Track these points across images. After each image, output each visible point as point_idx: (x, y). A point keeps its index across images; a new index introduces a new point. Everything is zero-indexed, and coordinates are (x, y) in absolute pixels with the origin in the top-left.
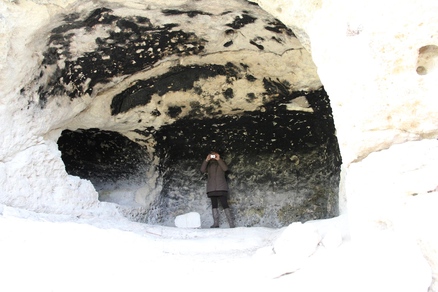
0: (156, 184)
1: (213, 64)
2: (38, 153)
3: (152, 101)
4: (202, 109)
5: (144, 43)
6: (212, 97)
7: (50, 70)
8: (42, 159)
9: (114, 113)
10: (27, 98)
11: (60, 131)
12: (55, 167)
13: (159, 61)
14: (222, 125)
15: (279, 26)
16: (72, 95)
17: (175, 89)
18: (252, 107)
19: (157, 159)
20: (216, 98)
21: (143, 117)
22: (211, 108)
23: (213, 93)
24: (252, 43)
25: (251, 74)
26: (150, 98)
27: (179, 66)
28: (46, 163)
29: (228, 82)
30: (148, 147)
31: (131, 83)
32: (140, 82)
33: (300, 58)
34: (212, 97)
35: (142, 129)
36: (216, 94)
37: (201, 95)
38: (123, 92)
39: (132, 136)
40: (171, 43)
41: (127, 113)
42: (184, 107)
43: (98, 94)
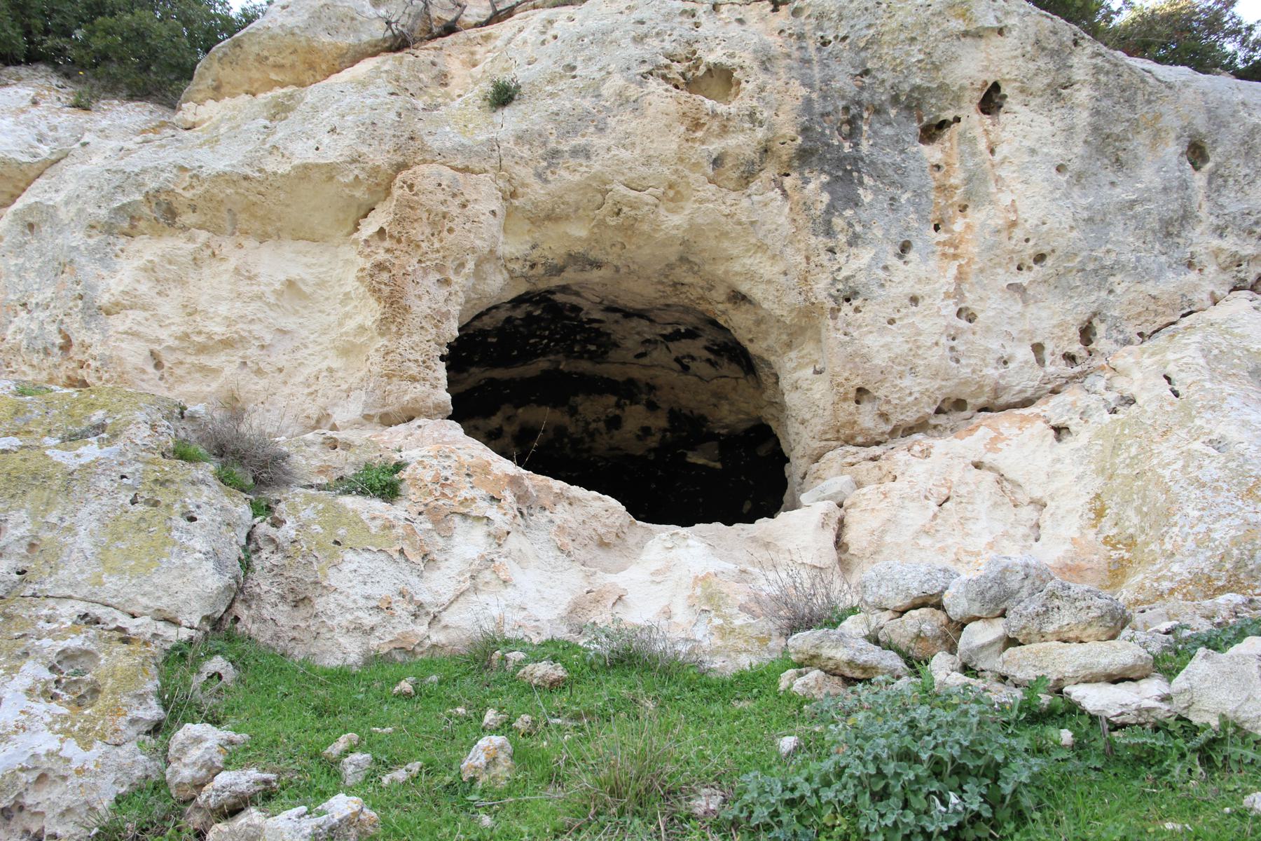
3: (499, 414)
4: (566, 440)
6: (588, 423)
15: (529, 355)
17: (541, 403)
18: (638, 449)
22: (581, 440)
23: (590, 417)
24: (677, 360)
25: (655, 399)
26: (498, 409)
27: (557, 370)
29: (618, 405)
33: (734, 389)
34: (588, 423)
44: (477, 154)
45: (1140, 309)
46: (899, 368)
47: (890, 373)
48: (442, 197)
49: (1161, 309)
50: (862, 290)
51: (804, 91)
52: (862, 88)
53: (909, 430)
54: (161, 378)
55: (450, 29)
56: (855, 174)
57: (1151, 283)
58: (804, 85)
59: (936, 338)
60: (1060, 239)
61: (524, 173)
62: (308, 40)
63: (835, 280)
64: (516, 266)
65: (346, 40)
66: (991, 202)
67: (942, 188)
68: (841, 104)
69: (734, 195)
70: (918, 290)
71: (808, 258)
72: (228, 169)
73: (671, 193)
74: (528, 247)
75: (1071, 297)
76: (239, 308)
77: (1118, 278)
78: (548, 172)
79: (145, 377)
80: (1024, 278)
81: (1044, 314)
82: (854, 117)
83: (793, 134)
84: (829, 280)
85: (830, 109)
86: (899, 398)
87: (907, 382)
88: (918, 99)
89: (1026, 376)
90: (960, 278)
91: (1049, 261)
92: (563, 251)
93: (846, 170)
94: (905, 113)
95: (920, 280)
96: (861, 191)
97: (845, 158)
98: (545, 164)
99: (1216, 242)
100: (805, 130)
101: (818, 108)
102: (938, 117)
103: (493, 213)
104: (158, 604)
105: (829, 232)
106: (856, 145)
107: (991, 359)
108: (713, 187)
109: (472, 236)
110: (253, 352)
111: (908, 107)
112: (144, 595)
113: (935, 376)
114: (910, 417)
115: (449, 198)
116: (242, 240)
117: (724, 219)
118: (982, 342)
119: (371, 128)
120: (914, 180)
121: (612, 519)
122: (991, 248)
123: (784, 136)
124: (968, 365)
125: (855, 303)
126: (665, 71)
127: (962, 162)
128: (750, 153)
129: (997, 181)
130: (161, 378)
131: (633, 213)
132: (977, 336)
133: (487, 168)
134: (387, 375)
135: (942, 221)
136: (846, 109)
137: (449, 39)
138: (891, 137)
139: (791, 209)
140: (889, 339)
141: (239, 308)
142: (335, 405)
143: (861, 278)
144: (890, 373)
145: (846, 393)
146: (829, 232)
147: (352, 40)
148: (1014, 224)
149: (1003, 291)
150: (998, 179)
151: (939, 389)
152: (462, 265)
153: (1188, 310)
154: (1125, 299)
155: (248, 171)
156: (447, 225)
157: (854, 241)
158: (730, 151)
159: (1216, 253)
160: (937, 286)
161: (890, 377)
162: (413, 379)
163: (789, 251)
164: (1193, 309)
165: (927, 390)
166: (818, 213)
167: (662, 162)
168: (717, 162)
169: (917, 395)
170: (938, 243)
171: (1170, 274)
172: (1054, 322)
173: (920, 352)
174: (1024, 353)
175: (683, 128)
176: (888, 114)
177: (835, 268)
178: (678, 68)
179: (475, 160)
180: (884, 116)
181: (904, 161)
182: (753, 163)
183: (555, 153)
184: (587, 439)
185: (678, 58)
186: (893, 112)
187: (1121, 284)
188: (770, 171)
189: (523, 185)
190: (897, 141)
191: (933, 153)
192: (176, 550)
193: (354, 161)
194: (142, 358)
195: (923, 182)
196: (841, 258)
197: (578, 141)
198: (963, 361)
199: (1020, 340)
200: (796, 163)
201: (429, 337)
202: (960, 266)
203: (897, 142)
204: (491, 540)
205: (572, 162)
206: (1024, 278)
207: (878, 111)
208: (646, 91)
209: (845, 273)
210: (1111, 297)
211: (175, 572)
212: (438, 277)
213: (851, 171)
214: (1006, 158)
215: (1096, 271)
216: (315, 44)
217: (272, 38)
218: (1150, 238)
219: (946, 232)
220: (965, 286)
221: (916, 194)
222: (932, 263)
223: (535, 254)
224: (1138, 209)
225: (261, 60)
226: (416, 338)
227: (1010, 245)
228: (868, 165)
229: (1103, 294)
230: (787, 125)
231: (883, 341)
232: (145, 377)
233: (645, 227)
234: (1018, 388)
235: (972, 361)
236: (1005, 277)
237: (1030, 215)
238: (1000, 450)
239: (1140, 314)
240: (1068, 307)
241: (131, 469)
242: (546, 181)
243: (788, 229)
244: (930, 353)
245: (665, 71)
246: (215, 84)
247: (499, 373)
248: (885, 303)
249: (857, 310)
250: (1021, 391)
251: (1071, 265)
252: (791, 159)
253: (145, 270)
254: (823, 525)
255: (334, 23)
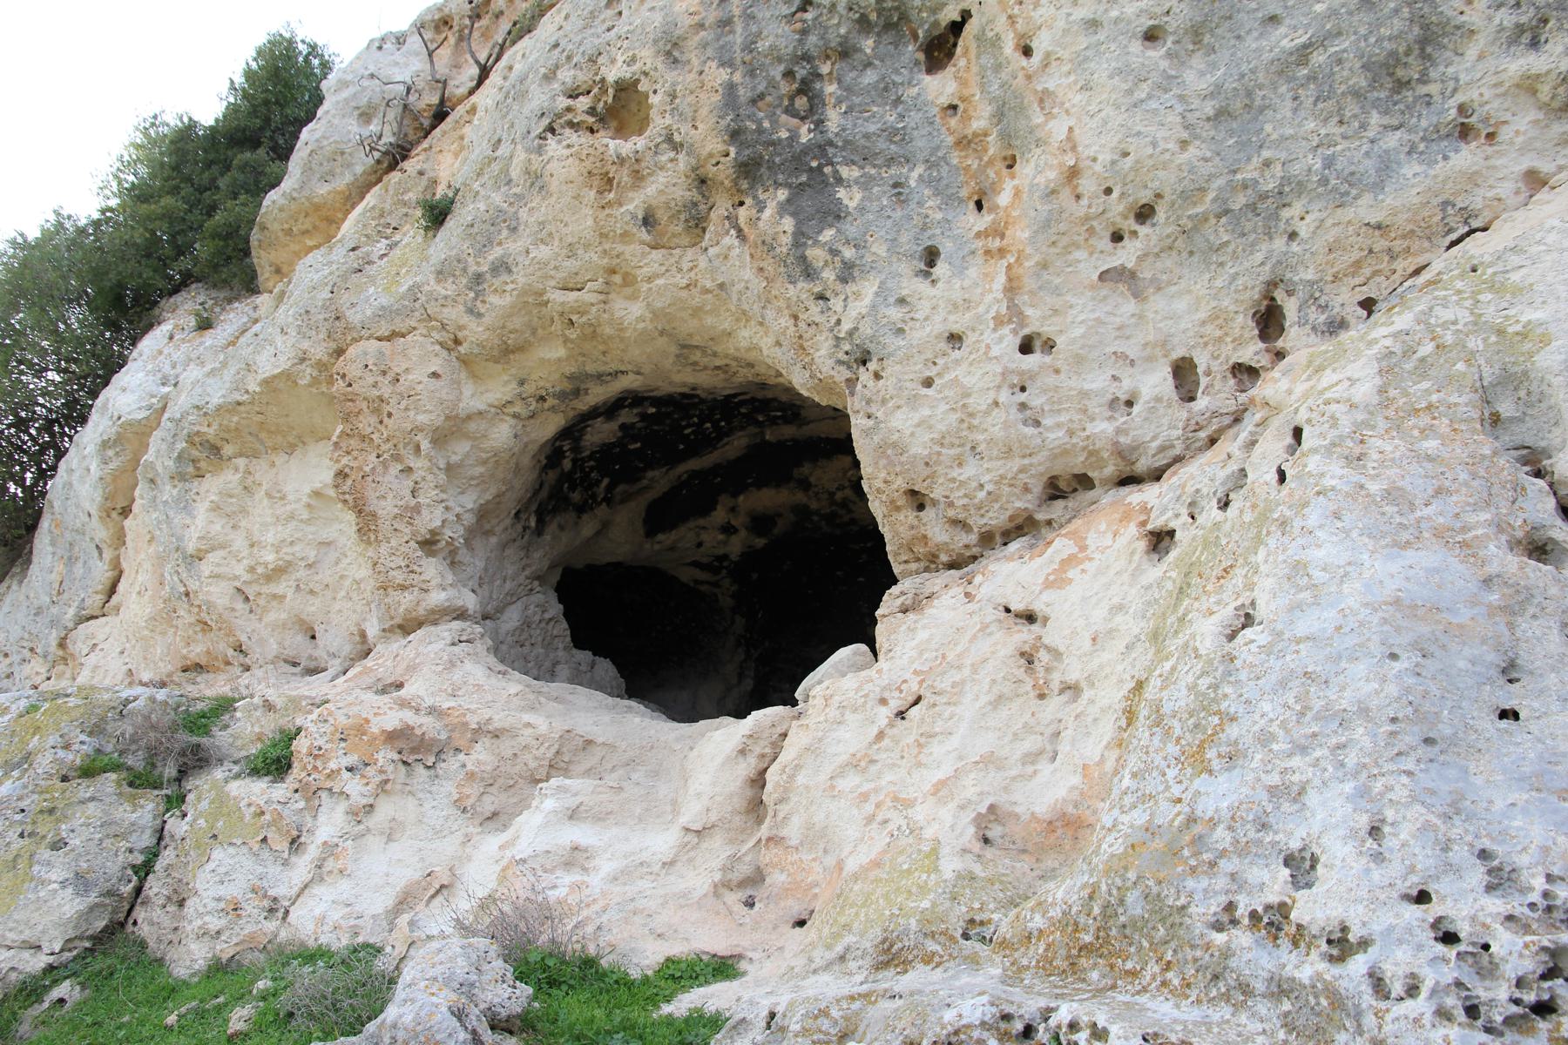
0: (741, 676)
1: (823, 436)
2: (532, 607)
3: (719, 507)
5: (696, 420)
6: (832, 494)
7: (552, 476)
8: (537, 618)
9: (650, 533)
10: (522, 523)
11: (559, 570)
12: (555, 632)
13: (726, 440)
14: (869, 545)
16: (581, 509)
17: (760, 485)
19: (740, 622)
20: (839, 496)
21: (705, 537)
26: (716, 503)
28: (543, 625)
30: (720, 596)
31: (680, 477)
32: (694, 474)
34: (832, 494)
35: (705, 560)
36: (838, 489)
37: (810, 493)
38: (665, 494)
39: (686, 575)
40: (740, 413)
41: (674, 532)
42: (780, 515)
43: (623, 501)
44: (398, 312)
45: (1356, 255)
46: (952, 452)
47: (938, 463)
48: (371, 380)
49: (1398, 245)
50: (872, 347)
51: (723, 75)
52: (804, 32)
53: (1008, 536)
54: (251, 611)
55: (440, 115)
56: (828, 170)
57: (1367, 199)
58: (722, 65)
59: (992, 395)
60: (1161, 174)
61: (455, 314)
62: (308, 199)
63: (837, 338)
64: (518, 408)
65: (343, 181)
66: (1038, 143)
67: (963, 143)
68: (777, 72)
69: (690, 253)
70: (956, 324)
71: (796, 318)
72: (221, 400)
73: (617, 279)
74: (514, 385)
75: (1221, 264)
76: (286, 532)
77: (1296, 209)
78: (478, 303)
79: (237, 614)
80: (1126, 255)
81: (1181, 305)
82: (803, 81)
83: (721, 147)
84: (831, 342)
85: (761, 88)
86: (966, 496)
87: (970, 470)
88: (897, 8)
89: (1165, 421)
90: (1011, 289)
91: (1161, 215)
92: (557, 376)
93: (811, 169)
94: (888, 38)
95: (955, 306)
96: (841, 193)
97: (806, 150)
98: (472, 295)
99: (1521, 63)
100: (735, 135)
101: (743, 94)
102: (936, 24)
103: (435, 375)
104: (23, 937)
105: (809, 273)
106: (819, 123)
107: (1095, 406)
108: (657, 255)
109: (412, 413)
110: (302, 573)
111: (888, 26)
112: (10, 930)
113: (1008, 453)
114: (996, 518)
115: (380, 378)
116: (273, 457)
117: (684, 294)
118: (1072, 383)
119: (305, 317)
120: (920, 143)
121: (542, 750)
122: (1047, 224)
123: (711, 155)
124: (1058, 425)
125: (872, 366)
126: (569, 116)
127: (983, 87)
128: (682, 192)
129: (1041, 101)
130: (251, 611)
131: (584, 319)
132: (1062, 376)
133: (413, 324)
134: (381, 587)
135: (982, 193)
136: (789, 74)
137: (443, 126)
138: (875, 86)
139: (752, 256)
140: (926, 412)
141: (286, 532)
142: (364, 620)
143: (866, 329)
144: (938, 463)
145: (892, 502)
146: (809, 273)
147: (348, 178)
148: (1073, 173)
149: (1092, 287)
150: (1044, 98)
151: (1021, 471)
152: (418, 448)
153: (1464, 229)
154: (1319, 245)
155: (238, 397)
156: (387, 408)
157: (847, 273)
158: (654, 203)
159: (1529, 85)
160: (981, 309)
161: (940, 470)
162: (403, 588)
163: (770, 314)
164: (1475, 224)
165: (1002, 477)
166: (784, 250)
167: (587, 247)
168: (648, 221)
169: (990, 487)
170: (978, 235)
171: (1411, 169)
172: (1202, 315)
173: (976, 422)
174: (1156, 382)
175: (593, 193)
176: (860, 50)
177: (833, 320)
178: (583, 103)
179: (398, 320)
180: (857, 56)
181: (902, 117)
182: (695, 204)
183: (478, 278)
184: (842, 512)
185: (584, 87)
186: (868, 44)
187: (1304, 216)
188: (722, 207)
189: (461, 328)
190: (886, 91)
191: (939, 87)
192: (32, 885)
193: (303, 360)
194: (228, 597)
195: (936, 141)
196: (836, 304)
197: (496, 253)
198: (1047, 421)
199: (1150, 359)
200: (745, 185)
201: (406, 538)
202: (1009, 267)
203: (886, 89)
204: (350, 817)
205: (497, 282)
206: (1126, 255)
207: (845, 52)
208: (545, 158)
209: (846, 326)
210: (1295, 247)
211: (32, 907)
212: (400, 467)
213: (820, 168)
214: (1048, 55)
215: (1252, 207)
216: (316, 200)
217: (281, 210)
218: (1352, 108)
219: (990, 211)
220: (1022, 299)
221: (930, 165)
222: (973, 272)
223: (529, 389)
224: (1319, 58)
225: (289, 232)
226: (394, 543)
227: (1080, 209)
228: (843, 149)
229: (1279, 243)
230: (708, 139)
231: (916, 417)
232: (237, 614)
233: (608, 331)
234: (1155, 444)
235: (1063, 418)
236: (1089, 266)
237: (1098, 148)
238: (1071, 581)
239: (1357, 264)
240: (1219, 283)
241: (28, 802)
242: (480, 315)
243: (758, 284)
244: (989, 419)
245: (569, 116)
246: (273, 269)
247: (694, 464)
248: (908, 358)
249: (877, 376)
250: (1162, 449)
251: (1199, 209)
252: (735, 182)
253: (214, 510)
254: (742, 752)
255: (327, 167)
